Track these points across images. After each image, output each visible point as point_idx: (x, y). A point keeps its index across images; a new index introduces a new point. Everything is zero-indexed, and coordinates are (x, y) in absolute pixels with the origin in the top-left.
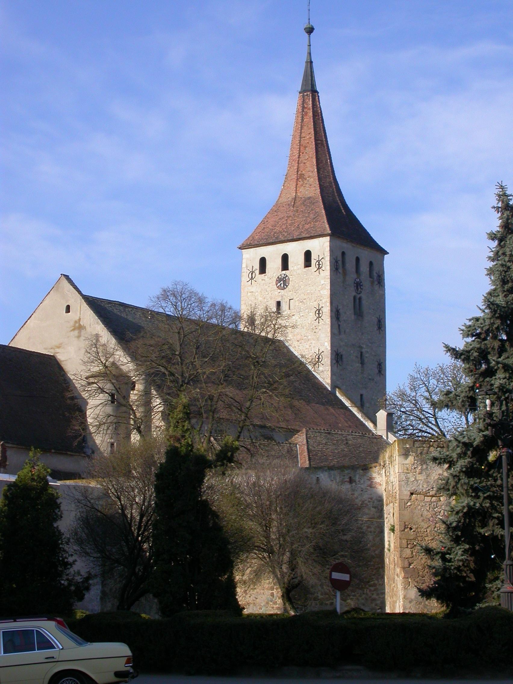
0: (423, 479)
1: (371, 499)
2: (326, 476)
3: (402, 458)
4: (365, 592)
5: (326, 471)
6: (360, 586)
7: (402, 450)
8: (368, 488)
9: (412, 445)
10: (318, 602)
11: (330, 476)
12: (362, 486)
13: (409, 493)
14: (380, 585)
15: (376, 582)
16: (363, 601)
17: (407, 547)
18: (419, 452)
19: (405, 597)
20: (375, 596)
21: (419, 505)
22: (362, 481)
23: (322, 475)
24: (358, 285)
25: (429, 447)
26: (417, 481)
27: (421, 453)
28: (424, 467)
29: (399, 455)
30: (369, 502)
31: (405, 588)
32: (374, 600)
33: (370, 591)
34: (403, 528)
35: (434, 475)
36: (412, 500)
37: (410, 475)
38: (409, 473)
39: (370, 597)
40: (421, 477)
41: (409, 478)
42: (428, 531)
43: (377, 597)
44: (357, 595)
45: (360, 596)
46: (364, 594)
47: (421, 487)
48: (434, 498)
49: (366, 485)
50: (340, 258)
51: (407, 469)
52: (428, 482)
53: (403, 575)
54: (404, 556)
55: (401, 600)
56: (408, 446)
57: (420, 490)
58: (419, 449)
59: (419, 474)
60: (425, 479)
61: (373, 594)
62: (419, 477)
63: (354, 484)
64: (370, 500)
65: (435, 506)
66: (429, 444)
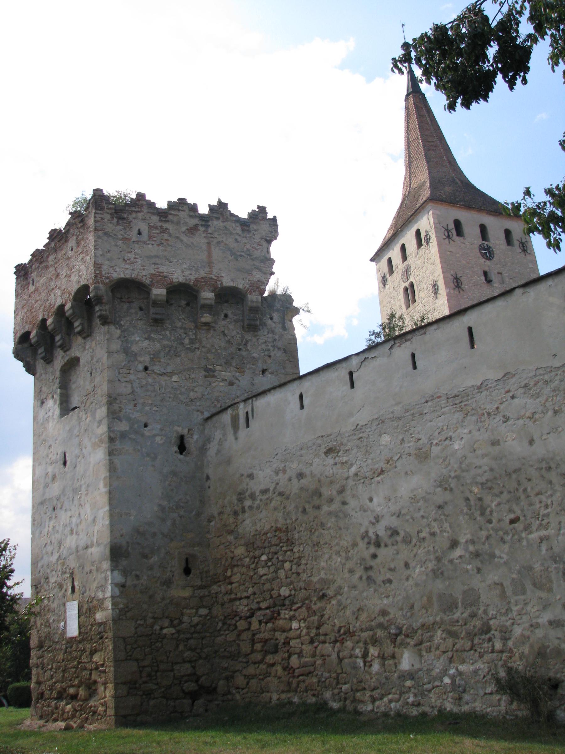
24: (487, 253)
50: (452, 226)
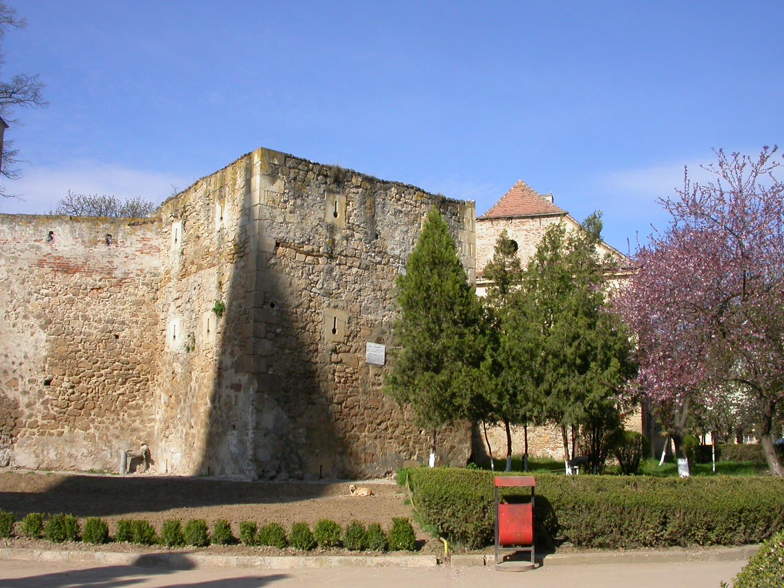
0: (295, 221)
1: (142, 270)
2: (67, 231)
3: (267, 181)
4: (121, 417)
5: (67, 222)
6: (113, 408)
7: (267, 167)
8: (138, 253)
9: (282, 162)
10: (35, 430)
11: (72, 232)
12: (128, 250)
13: (274, 243)
14: (146, 406)
15: (141, 402)
16: (117, 432)
17: (265, 338)
18: (292, 175)
19: (257, 428)
20: (137, 424)
21: (288, 265)
22: (128, 243)
23: (58, 228)
25: (307, 171)
26: (287, 223)
27: (295, 179)
28: (299, 202)
29: (263, 175)
30: (137, 275)
31: (258, 411)
32: (135, 430)
33: (130, 415)
34: (261, 303)
35: (312, 218)
36: (278, 256)
37: (277, 212)
38: (275, 208)
39: (130, 425)
40: (293, 219)
41: (275, 217)
42: (299, 313)
43: (141, 426)
44: (107, 422)
45: (112, 424)
46: (118, 419)
47: (291, 234)
48: (309, 258)
49: (134, 249)
51: (274, 201)
52: (302, 229)
53: (256, 385)
54: (260, 351)
55: (251, 431)
56: (276, 163)
57: (291, 241)
58: (292, 171)
59: (291, 212)
60: (298, 223)
61: (134, 421)
62: (291, 218)
63: (113, 246)
64: (139, 272)
65: (311, 272)
66: (308, 166)
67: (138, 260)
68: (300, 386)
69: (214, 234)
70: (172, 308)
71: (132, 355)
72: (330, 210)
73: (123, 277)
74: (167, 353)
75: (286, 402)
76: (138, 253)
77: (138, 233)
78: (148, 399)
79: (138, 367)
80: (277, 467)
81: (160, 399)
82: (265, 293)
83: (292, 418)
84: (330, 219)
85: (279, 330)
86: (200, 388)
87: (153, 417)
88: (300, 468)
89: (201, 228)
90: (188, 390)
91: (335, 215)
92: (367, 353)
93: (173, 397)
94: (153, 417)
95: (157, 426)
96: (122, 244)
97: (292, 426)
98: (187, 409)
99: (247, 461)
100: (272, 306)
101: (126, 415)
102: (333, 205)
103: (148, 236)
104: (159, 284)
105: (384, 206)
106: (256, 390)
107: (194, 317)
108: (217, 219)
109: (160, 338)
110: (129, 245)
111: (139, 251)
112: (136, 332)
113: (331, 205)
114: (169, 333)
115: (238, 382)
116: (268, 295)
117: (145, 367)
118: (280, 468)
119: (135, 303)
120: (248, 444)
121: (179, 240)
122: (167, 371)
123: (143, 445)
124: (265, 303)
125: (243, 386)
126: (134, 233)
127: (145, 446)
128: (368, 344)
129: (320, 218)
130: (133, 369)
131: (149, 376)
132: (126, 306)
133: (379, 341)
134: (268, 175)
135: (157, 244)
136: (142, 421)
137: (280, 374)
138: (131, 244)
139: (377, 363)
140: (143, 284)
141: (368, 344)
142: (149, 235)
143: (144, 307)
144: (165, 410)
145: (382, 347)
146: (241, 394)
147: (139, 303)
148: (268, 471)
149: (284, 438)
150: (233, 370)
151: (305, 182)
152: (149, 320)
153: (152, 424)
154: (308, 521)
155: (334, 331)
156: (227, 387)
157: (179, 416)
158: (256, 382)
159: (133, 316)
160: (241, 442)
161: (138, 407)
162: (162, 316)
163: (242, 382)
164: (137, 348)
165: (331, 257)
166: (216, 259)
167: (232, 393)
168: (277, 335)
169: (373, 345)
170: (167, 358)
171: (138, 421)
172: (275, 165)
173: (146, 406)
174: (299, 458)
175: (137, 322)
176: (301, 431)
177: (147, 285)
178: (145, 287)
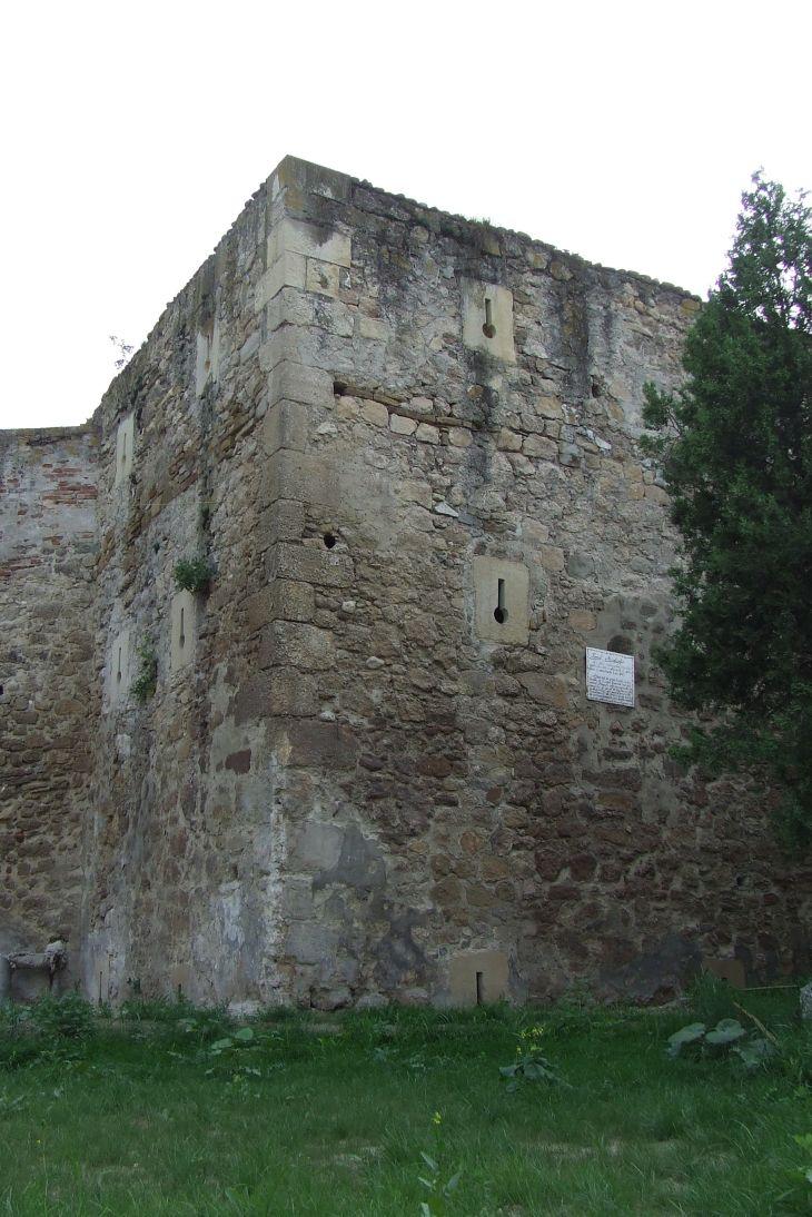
1: (56, 540)
12: (26, 498)
15: (50, 838)
22: (25, 483)
33: (24, 870)
64: (49, 544)
67: (48, 518)
68: (412, 753)
69: (193, 407)
70: (118, 612)
71: (31, 730)
72: (474, 317)
73: (14, 556)
74: (105, 717)
75: (372, 798)
76: (48, 503)
77: (47, 460)
78: (66, 831)
79: (46, 757)
80: (351, 977)
81: (91, 828)
82: (307, 506)
83: (394, 839)
84: (474, 338)
85: (349, 604)
86: (164, 782)
87: (79, 872)
88: (421, 980)
89: (169, 407)
90: (143, 796)
91: (488, 330)
92: (590, 673)
93: (116, 818)
94: (79, 872)
95: (84, 893)
96: (12, 485)
97: (390, 862)
98: (139, 840)
99: (265, 961)
100: (330, 541)
101: (15, 870)
102: (480, 307)
103: (71, 465)
104: (95, 568)
105: (609, 320)
106: (286, 762)
107: (155, 615)
108: (200, 362)
109: (94, 688)
110: (28, 486)
111: (50, 498)
112: (41, 676)
113: (474, 308)
114: (110, 673)
115: (242, 748)
116: (315, 512)
117: (62, 756)
118: (362, 981)
119: (39, 613)
120: (268, 913)
121: (129, 458)
122: (107, 758)
123: (52, 940)
124: (308, 532)
125: (253, 755)
126: (39, 460)
127: (58, 943)
128: (591, 652)
129: (447, 336)
130: (33, 762)
131: (69, 778)
132: (19, 620)
133: (618, 645)
134: (308, 220)
135: (90, 482)
136: (53, 885)
137: (354, 719)
138: (33, 483)
139: (617, 702)
140: (58, 570)
141: (591, 652)
142: (73, 462)
143: (61, 620)
144: (101, 853)
145: (628, 662)
146: (251, 779)
147: (48, 613)
148: (326, 990)
149: (371, 897)
150: (232, 720)
151: (407, 248)
152: (75, 648)
153: (77, 889)
154: (613, 631)
155: (500, 615)
156: (219, 768)
157: (123, 862)
158: (287, 741)
159: (34, 641)
160: (251, 913)
161: (42, 849)
162: (99, 636)
163: (252, 746)
164: (41, 714)
165: (482, 427)
166: (198, 462)
167: (230, 778)
168: (344, 617)
169: (605, 655)
170: (107, 727)
171: (43, 885)
172: (327, 200)
173: (62, 849)
174: (418, 952)
175: (43, 656)
176: (417, 876)
177: (67, 571)
178: (63, 577)
